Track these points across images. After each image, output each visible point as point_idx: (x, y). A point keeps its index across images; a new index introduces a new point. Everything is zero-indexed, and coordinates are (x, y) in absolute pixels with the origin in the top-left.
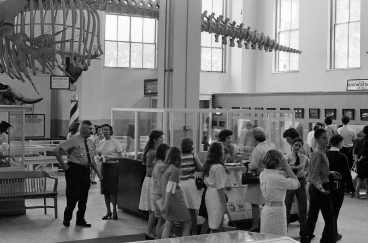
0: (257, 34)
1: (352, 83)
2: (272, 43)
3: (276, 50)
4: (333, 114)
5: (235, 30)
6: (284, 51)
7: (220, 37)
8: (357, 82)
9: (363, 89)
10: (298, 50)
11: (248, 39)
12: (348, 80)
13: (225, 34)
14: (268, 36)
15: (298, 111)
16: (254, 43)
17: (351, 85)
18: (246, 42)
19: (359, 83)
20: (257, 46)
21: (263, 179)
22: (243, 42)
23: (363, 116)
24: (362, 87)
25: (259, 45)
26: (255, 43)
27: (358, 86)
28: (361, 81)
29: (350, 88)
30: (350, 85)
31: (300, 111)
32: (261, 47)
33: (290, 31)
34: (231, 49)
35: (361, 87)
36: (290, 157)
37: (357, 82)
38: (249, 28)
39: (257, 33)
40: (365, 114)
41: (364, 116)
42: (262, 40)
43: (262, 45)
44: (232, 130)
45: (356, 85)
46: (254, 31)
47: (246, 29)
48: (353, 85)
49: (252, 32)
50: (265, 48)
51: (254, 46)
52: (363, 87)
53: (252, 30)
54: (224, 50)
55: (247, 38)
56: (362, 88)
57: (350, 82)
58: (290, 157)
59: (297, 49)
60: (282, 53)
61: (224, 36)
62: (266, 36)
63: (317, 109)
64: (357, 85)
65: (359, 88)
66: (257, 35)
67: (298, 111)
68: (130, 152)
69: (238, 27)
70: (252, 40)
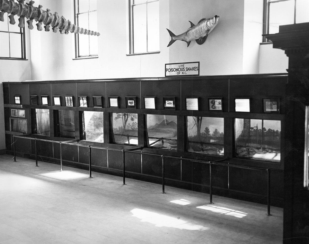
0: (50, 13)
2: (67, 25)
5: (23, 7)
7: (16, 17)
8: (176, 66)
12: (166, 64)
13: (11, 12)
16: (47, 25)
18: (10, 14)
20: (51, 28)
22: (34, 23)
24: (183, 71)
26: (49, 24)
28: (180, 64)
29: (168, 74)
32: (55, 28)
34: (30, 31)
36: (133, 214)
38: (40, 7)
39: (50, 12)
42: (56, 21)
43: (57, 26)
44: (189, 126)
45: (175, 70)
46: (46, 10)
47: (37, 8)
48: (171, 70)
49: (44, 12)
50: (60, 30)
53: (43, 9)
54: (23, 34)
55: (39, 18)
56: (183, 73)
57: (168, 67)
58: (133, 214)
61: (10, 14)
64: (177, 70)
65: (179, 73)
66: (49, 15)
69: (27, 5)
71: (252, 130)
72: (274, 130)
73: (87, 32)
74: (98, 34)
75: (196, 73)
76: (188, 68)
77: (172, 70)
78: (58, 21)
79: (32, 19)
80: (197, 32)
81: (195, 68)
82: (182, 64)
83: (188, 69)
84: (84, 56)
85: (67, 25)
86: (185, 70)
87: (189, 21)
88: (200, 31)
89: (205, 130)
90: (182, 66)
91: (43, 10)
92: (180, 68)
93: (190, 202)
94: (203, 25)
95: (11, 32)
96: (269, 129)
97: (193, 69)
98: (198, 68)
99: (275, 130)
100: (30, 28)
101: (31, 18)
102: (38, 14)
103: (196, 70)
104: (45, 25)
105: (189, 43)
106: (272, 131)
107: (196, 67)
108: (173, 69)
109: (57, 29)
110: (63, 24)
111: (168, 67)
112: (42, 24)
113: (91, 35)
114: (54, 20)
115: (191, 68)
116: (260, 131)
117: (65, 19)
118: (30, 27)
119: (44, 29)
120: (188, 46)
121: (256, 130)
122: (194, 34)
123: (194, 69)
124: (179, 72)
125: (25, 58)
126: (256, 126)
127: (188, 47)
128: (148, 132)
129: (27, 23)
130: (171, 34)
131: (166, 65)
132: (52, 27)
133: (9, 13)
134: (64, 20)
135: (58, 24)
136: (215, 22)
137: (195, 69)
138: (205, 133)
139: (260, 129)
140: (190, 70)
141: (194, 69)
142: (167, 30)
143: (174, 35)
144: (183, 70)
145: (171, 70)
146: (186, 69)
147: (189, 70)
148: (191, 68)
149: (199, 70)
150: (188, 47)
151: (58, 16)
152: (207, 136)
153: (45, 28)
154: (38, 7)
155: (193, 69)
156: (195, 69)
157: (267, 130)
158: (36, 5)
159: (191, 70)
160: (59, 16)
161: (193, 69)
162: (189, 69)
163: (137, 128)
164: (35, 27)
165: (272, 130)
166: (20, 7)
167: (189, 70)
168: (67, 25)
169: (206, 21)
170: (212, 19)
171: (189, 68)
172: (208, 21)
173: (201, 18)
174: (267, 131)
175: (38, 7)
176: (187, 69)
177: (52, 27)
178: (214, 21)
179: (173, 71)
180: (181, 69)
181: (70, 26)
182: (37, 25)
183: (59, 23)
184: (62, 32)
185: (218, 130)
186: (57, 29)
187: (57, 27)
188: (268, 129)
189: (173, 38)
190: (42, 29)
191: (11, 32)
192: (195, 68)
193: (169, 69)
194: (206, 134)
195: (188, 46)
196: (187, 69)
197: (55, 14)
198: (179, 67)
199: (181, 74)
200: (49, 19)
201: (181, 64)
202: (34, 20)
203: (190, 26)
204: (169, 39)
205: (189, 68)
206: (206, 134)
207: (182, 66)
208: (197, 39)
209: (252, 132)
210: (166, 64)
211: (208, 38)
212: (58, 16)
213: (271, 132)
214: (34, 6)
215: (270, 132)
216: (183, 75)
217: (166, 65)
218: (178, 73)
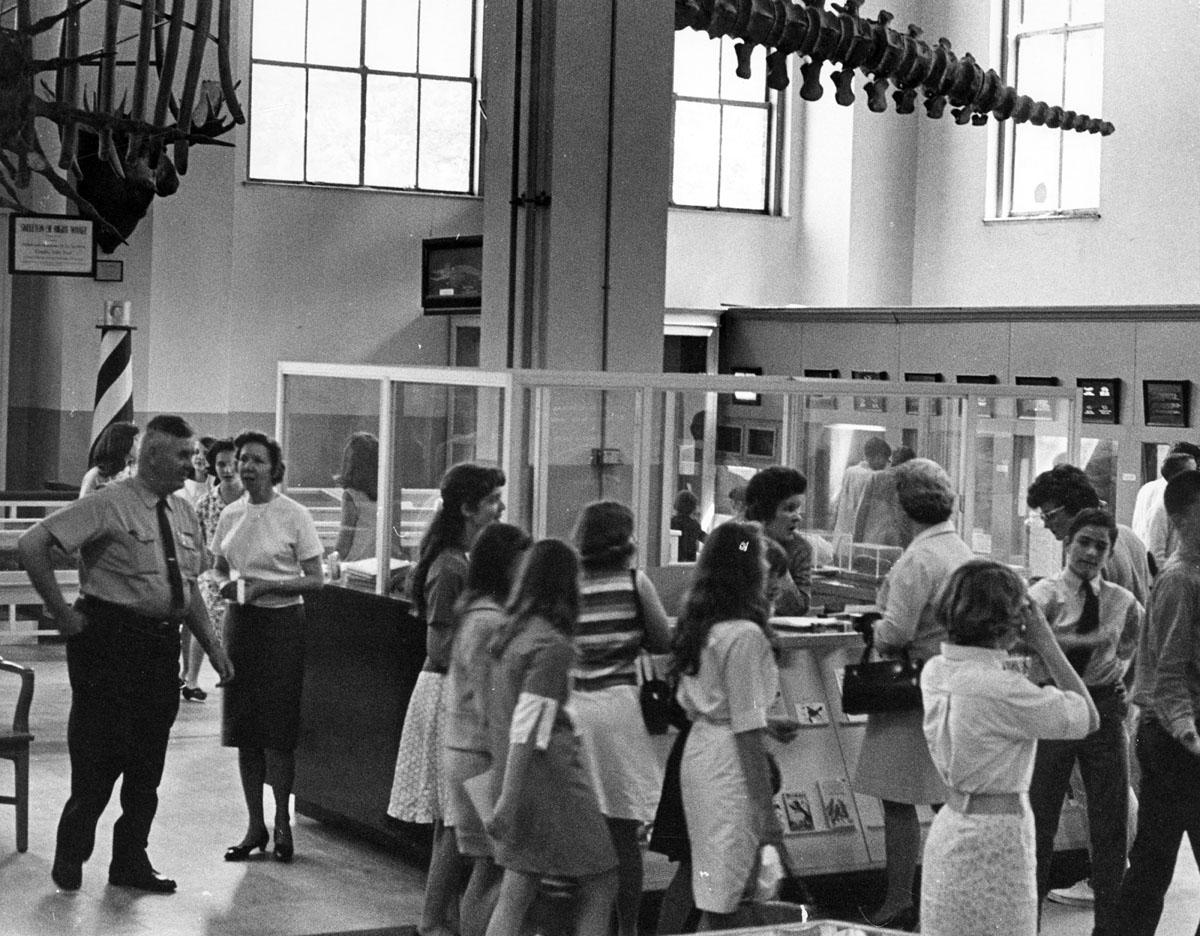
0: (922, 44)
2: (986, 86)
6: (1038, 121)
10: (1098, 121)
12: (121, 280)
14: (968, 55)
15: (1097, 391)
20: (920, 99)
25: (926, 94)
26: (914, 83)
31: (1105, 392)
34: (804, 107)
38: (885, 17)
39: (921, 38)
42: (941, 72)
47: (873, 22)
49: (898, 37)
50: (953, 108)
54: (775, 114)
60: (1028, 133)
66: (919, 49)
67: (1097, 391)
69: (836, 13)
73: (1060, 117)
74: (1106, 129)
84: (605, 207)
87: (1022, 22)
91: (894, 31)
95: (314, 67)
101: (848, 61)
102: (874, 48)
104: (897, 89)
109: (944, 103)
112: (888, 85)
113: (1077, 131)
114: (935, 68)
117: (977, 66)
118: (811, 91)
119: (923, 110)
125: (779, 212)
132: (925, 99)
133: (735, 36)
134: (975, 68)
135: (948, 83)
153: (871, 95)
154: (875, 18)
158: (868, 12)
163: (1113, 635)
166: (810, 24)
175: (875, 18)
177: (925, 99)
182: (868, 88)
190: (886, 105)
191: (314, 67)
197: (942, 46)
202: (858, 71)
210: (121, 280)
214: (861, 16)
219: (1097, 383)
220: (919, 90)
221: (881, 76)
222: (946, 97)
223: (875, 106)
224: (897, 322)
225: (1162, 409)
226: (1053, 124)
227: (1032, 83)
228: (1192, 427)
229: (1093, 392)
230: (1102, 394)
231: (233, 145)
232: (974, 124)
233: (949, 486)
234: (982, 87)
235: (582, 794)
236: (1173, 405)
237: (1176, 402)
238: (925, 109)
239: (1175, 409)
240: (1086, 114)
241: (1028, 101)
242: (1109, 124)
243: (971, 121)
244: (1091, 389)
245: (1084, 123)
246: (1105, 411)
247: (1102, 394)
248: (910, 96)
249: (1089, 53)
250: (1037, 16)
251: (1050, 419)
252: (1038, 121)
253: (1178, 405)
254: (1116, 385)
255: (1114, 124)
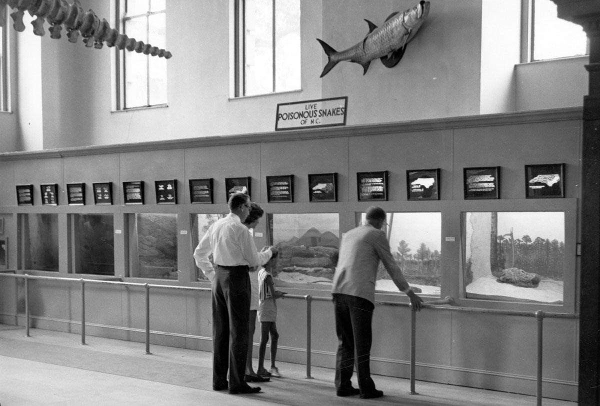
1: (294, 120)
2: (101, 27)
3: (110, 44)
4: (245, 189)
6: (139, 50)
8: (301, 108)
9: (315, 124)
10: (163, 51)
11: (40, 10)
12: (278, 105)
14: (104, 19)
15: (165, 187)
17: (285, 117)
18: (35, 17)
19: (304, 111)
20: (64, 32)
21: (209, 378)
23: (316, 192)
24: (313, 118)
25: (68, 29)
26: (60, 22)
27: (302, 119)
28: (308, 104)
29: (282, 124)
30: (282, 116)
31: (170, 187)
32: (74, 34)
33: (149, 13)
35: (309, 119)
37: (301, 108)
40: (321, 186)
41: (318, 190)
42: (75, 17)
43: (77, 29)
45: (296, 116)
48: (290, 116)
50: (83, 39)
51: (55, 29)
52: (315, 119)
55: (38, 8)
56: (312, 122)
57: (283, 110)
59: (161, 46)
60: (134, 59)
62: (102, 21)
63: (207, 180)
64: (301, 115)
65: (305, 122)
67: (165, 187)
68: (258, 285)
70: (50, 13)
71: (502, 241)
72: (548, 240)
73: (142, 47)
75: (339, 119)
76: (323, 112)
77: (290, 117)
78: (81, 19)
79: (22, 9)
80: (383, 41)
81: (338, 110)
82: (312, 104)
83: (324, 113)
85: (99, 30)
86: (318, 114)
88: (388, 38)
89: (398, 248)
90: (312, 108)
92: (308, 111)
93: (481, 185)
94: (396, 22)
96: (538, 238)
97: (334, 112)
98: (343, 110)
99: (551, 240)
100: (16, 28)
103: (339, 115)
105: (366, 67)
106: (544, 243)
107: (340, 108)
108: (293, 115)
110: (92, 24)
111: (283, 110)
112: (44, 21)
114: (72, 15)
115: (330, 111)
116: (518, 242)
117: (96, 16)
120: (365, 71)
121: (510, 240)
122: (375, 45)
123: (336, 112)
124: (304, 119)
126: (510, 233)
127: (364, 74)
128: (306, 231)
129: (11, 18)
130: (328, 49)
131: (280, 107)
134: (95, 17)
135: (80, 24)
136: (421, 14)
137: (339, 113)
138: (399, 252)
139: (518, 238)
140: (328, 114)
141: (336, 112)
142: (318, 42)
143: (333, 51)
144: (314, 115)
145: (290, 116)
146: (320, 113)
147: (325, 114)
148: (330, 111)
149: (345, 114)
150: (364, 74)
151: (81, 8)
152: (403, 260)
155: (334, 112)
156: (337, 111)
157: (533, 240)
159: (330, 114)
160: (82, 8)
161: (334, 112)
162: (325, 113)
164: (29, 28)
165: (543, 240)
167: (325, 114)
168: (99, 30)
169: (402, 15)
170: (414, 9)
171: (326, 110)
172: (406, 13)
173: (391, 12)
174: (532, 242)
176: (322, 112)
178: (418, 12)
179: (293, 117)
180: (309, 114)
181: (107, 32)
183: (82, 22)
184: (89, 44)
185: (427, 247)
186: (78, 34)
187: (76, 31)
188: (534, 240)
189: (333, 58)
192: (338, 110)
193: (307, 117)
194: (401, 255)
195: (365, 71)
196: (322, 112)
198: (306, 109)
199: (308, 124)
200: (60, 11)
201: (310, 104)
202: (26, 12)
203: (368, 29)
204: (322, 59)
205: (326, 110)
206: (401, 255)
207: (312, 108)
208: (384, 55)
209: (501, 245)
211: (406, 51)
212: (81, 8)
213: (542, 243)
215: (538, 243)
216: (312, 125)
217: (280, 107)
218: (303, 122)
219: (165, 183)
220: (63, 26)
221: (41, 16)
222: (79, 32)
223: (37, 32)
224: (62, 157)
225: (199, 194)
226: (147, 53)
227: (134, 32)
228: (216, 203)
229: (163, 188)
230: (168, 188)
231: (439, 199)
232: (96, 48)
233: (578, 199)
234: (98, 28)
235: (389, 257)
236: (205, 192)
237: (206, 190)
238: (49, 33)
239: (206, 194)
240: (156, 46)
241: (133, 40)
242: (169, 53)
243: (94, 46)
244: (163, 186)
245: (155, 51)
246: (170, 197)
247: (168, 188)
248: (58, 29)
249: (159, 22)
250: (137, 3)
251: (82, 204)
252: (139, 51)
253: (208, 192)
254: (175, 183)
255: (171, 53)
